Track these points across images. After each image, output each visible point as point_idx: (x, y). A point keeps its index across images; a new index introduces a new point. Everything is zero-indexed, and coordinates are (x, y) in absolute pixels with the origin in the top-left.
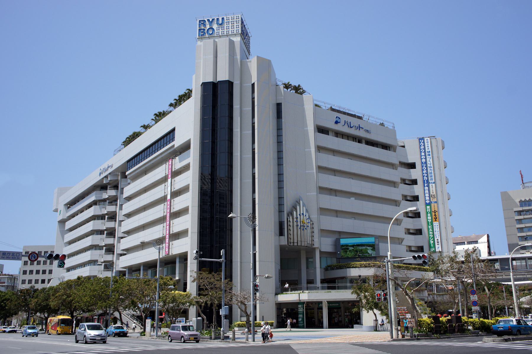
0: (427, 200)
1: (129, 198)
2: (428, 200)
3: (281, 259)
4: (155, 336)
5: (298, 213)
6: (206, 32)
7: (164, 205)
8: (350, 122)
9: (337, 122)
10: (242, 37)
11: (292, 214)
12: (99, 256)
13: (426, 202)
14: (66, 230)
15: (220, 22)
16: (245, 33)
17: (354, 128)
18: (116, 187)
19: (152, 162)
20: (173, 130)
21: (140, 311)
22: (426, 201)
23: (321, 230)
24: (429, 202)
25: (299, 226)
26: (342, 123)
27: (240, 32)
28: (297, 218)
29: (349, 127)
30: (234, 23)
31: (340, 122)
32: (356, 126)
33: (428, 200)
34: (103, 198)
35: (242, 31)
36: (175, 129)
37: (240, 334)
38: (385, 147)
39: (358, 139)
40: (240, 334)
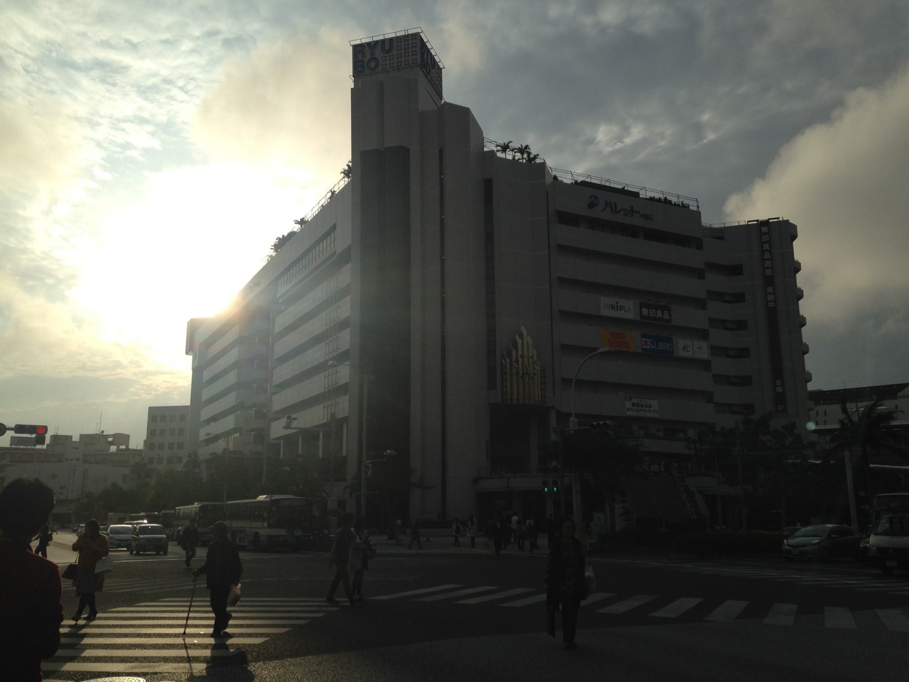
0: (770, 301)
2: (773, 301)
5: (520, 353)
6: (366, 66)
9: (591, 205)
10: (424, 70)
11: (509, 355)
13: (769, 306)
15: (387, 47)
16: (429, 63)
21: (252, 657)
22: (766, 271)
24: (774, 305)
25: (521, 374)
27: (419, 61)
28: (517, 361)
30: (408, 48)
33: (773, 301)
37: (234, 615)
38: (682, 240)
40: (234, 615)
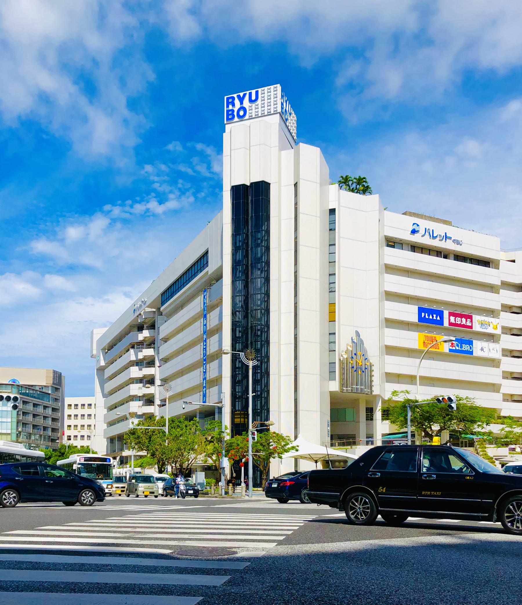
1: (165, 340)
3: (331, 410)
4: (466, 323)
7: (201, 346)
8: (433, 230)
9: (414, 232)
12: (138, 407)
14: (106, 379)
17: (438, 238)
18: (152, 326)
19: (187, 294)
20: (207, 253)
23: (386, 373)
26: (422, 232)
29: (432, 236)
31: (418, 231)
32: (440, 236)
34: (139, 340)
35: (282, 108)
36: (208, 251)
39: (444, 253)
